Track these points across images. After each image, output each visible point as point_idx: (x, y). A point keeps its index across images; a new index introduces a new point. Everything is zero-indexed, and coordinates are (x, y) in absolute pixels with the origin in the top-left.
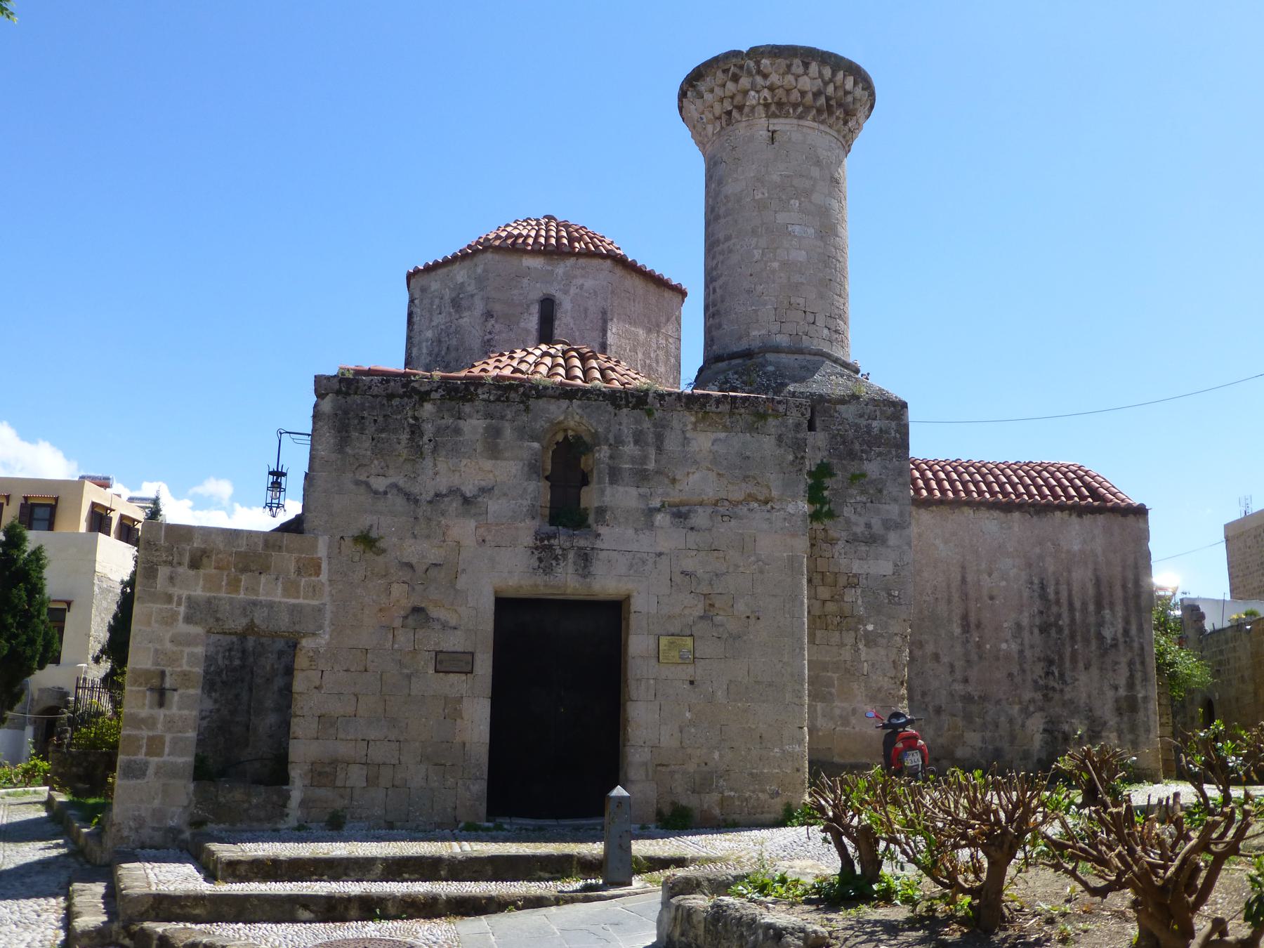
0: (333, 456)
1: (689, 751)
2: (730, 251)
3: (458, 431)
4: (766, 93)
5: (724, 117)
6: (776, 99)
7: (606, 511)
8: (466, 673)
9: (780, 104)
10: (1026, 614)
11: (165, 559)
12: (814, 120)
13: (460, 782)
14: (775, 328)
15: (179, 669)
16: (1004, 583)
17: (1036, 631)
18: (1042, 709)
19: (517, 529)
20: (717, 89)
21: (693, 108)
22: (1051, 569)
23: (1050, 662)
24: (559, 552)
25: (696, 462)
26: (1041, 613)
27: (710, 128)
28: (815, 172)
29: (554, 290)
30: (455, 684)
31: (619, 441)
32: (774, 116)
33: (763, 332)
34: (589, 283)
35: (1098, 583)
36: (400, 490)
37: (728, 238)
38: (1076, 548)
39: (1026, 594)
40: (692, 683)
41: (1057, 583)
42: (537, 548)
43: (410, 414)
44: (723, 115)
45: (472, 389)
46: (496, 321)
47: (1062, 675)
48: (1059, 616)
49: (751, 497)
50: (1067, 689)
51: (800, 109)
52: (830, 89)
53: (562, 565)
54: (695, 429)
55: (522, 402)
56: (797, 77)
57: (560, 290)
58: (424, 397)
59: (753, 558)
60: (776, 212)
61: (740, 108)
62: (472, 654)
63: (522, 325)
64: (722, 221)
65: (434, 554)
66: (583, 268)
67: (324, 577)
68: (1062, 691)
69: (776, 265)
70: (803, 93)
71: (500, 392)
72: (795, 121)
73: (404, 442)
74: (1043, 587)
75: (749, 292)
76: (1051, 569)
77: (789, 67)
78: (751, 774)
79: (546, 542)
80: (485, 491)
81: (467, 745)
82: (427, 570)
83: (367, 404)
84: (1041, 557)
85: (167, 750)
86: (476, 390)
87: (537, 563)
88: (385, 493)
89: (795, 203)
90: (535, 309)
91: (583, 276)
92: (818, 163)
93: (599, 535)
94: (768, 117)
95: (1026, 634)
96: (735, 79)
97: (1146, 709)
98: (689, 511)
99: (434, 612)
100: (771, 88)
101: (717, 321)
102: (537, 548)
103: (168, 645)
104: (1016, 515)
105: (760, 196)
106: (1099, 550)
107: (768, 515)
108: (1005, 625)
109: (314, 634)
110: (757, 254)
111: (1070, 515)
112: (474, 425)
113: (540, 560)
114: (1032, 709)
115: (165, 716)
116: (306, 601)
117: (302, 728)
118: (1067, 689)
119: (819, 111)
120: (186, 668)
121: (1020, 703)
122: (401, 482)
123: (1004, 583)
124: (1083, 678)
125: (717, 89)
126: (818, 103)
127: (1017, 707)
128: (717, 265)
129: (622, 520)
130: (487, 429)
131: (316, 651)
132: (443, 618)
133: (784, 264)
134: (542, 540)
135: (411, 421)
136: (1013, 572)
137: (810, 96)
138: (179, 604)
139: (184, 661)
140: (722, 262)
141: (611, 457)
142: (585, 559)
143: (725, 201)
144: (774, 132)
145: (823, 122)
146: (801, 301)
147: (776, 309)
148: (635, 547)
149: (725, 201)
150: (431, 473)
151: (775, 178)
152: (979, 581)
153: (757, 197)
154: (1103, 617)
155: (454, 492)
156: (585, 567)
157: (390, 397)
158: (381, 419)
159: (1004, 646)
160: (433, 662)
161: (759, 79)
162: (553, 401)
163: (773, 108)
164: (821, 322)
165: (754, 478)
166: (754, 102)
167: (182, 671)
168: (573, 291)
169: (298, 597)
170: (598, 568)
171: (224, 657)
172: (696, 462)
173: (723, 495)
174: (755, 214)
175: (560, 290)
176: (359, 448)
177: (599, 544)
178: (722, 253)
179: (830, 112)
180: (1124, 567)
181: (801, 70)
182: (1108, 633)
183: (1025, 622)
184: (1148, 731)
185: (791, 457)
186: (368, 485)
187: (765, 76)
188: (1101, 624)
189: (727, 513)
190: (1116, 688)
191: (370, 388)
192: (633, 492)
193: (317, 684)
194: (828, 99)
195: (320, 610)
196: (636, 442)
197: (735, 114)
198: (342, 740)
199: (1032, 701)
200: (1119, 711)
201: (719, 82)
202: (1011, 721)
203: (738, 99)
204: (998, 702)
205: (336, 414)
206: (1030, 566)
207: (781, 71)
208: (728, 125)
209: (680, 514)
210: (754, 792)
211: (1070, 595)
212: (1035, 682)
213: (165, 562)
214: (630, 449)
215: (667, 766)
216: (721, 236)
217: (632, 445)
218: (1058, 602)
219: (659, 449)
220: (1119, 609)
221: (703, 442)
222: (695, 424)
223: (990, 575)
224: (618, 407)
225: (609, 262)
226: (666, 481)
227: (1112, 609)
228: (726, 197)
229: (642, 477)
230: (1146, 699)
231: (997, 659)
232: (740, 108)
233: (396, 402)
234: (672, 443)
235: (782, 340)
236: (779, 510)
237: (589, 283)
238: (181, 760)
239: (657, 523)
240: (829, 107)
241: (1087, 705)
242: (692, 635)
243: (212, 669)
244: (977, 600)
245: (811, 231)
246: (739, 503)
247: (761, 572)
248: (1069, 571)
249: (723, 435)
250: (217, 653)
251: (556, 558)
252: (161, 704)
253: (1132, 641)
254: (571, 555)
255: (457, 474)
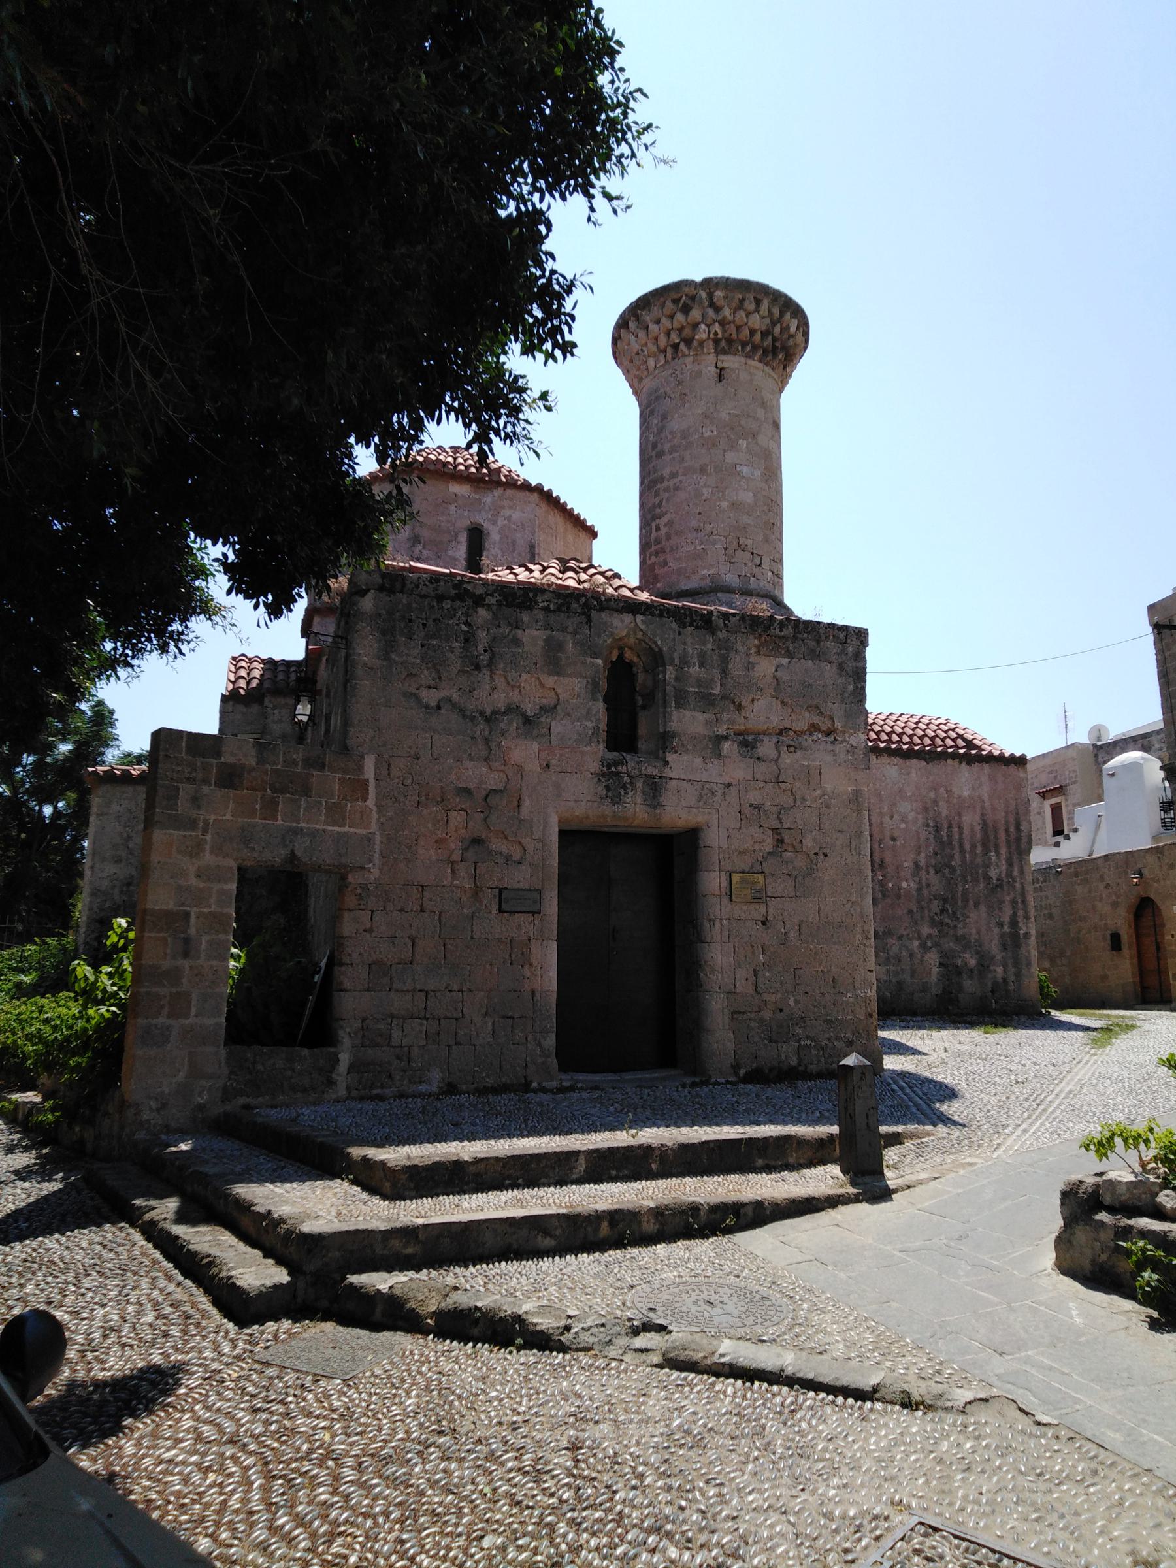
0: (378, 663)
1: (765, 996)
2: (677, 488)
3: (517, 642)
4: (717, 327)
5: (669, 350)
6: (726, 335)
7: (673, 737)
8: (533, 913)
9: (730, 341)
10: (923, 855)
11: (187, 775)
12: (760, 361)
13: (530, 1037)
14: (724, 568)
15: (206, 910)
16: (903, 826)
17: (932, 871)
18: (937, 945)
19: (583, 753)
20: (664, 320)
21: (632, 343)
22: (944, 813)
23: (945, 900)
24: (627, 780)
25: (760, 689)
26: (936, 854)
27: (651, 362)
28: (760, 413)
29: (481, 519)
30: (523, 925)
31: (685, 662)
32: (725, 353)
33: (712, 572)
34: (517, 515)
35: (984, 824)
36: (454, 705)
37: (674, 475)
38: (966, 793)
39: (923, 835)
40: (764, 923)
41: (950, 826)
42: (604, 775)
43: (463, 619)
44: (669, 349)
45: (531, 595)
46: (424, 548)
47: (954, 913)
48: (952, 857)
49: (814, 728)
50: (960, 925)
51: (748, 348)
52: (777, 330)
53: (631, 794)
54: (758, 653)
55: (584, 614)
56: (748, 314)
57: (489, 520)
58: (479, 601)
59: (818, 792)
60: (725, 451)
61: (688, 342)
62: (539, 891)
63: (450, 553)
64: (667, 458)
65: (494, 781)
66: (511, 500)
67: (371, 802)
68: (955, 927)
69: (725, 504)
70: (753, 332)
71: (560, 601)
72: (743, 360)
73: (458, 651)
74: (937, 830)
75: (697, 530)
76: (944, 813)
77: (742, 301)
78: (826, 1021)
79: (613, 769)
80: (548, 710)
81: (538, 995)
82: (487, 796)
83: (414, 605)
84: (936, 802)
85: (193, 1011)
86: (535, 596)
87: (605, 792)
88: (439, 707)
89: (743, 443)
90: (463, 538)
91: (510, 508)
92: (763, 405)
93: (667, 763)
94: (717, 353)
95: (923, 874)
96: (686, 310)
97: (1027, 945)
98: (755, 740)
99: (496, 845)
100: (723, 323)
101: (662, 559)
102: (604, 775)
103: (193, 881)
104: (914, 762)
105: (709, 433)
106: (986, 797)
107: (831, 748)
108: (905, 865)
109: (362, 868)
110: (706, 493)
111: (960, 763)
112: (532, 636)
113: (607, 788)
114: (929, 944)
115: (191, 967)
116: (352, 830)
117: (352, 978)
118: (960, 925)
119: (765, 352)
120: (213, 908)
121: (919, 938)
122: (455, 696)
123: (903, 826)
124: (973, 916)
125: (664, 320)
126: (765, 344)
127: (916, 943)
128: (661, 501)
129: (690, 747)
130: (548, 641)
131: (365, 888)
132: (505, 851)
133: (734, 505)
134: (609, 766)
135: (465, 628)
136: (911, 816)
137: (758, 337)
138: (205, 831)
139: (212, 901)
140: (668, 500)
141: (677, 679)
142: (655, 789)
143: (670, 437)
144: (722, 369)
145: (766, 364)
146: (749, 542)
147: (725, 549)
148: (704, 776)
149: (670, 437)
150: (487, 687)
151: (724, 416)
152: (882, 823)
153: (706, 435)
154: (990, 859)
155: (512, 710)
156: (654, 797)
157: (441, 598)
158: (430, 623)
159: (904, 885)
160: (497, 900)
161: (711, 312)
162: (616, 615)
163: (723, 343)
164: (765, 566)
165: (817, 707)
166: (704, 336)
167: (210, 913)
168: (501, 522)
169: (344, 825)
170: (668, 799)
171: (121, 892)
172: (760, 689)
173: (787, 724)
174: (703, 451)
175: (489, 520)
176: (407, 655)
177: (668, 773)
178: (667, 490)
179: (775, 354)
180: (1006, 813)
181: (752, 307)
182: (993, 873)
183: (922, 862)
184: (1029, 965)
185: (851, 687)
186: (418, 699)
187: (717, 310)
188: (987, 866)
189: (792, 743)
190: (1001, 925)
191: (417, 586)
192: (701, 717)
193: (368, 926)
194: (774, 340)
195: (369, 839)
196: (702, 665)
197: (682, 347)
198: (397, 991)
199: (929, 936)
200: (1004, 947)
201: (667, 311)
202: (912, 955)
203: (687, 332)
204: (900, 937)
205: (380, 615)
206: (926, 809)
207: (734, 305)
208: (673, 359)
209: (747, 742)
210: (829, 1040)
211: (961, 838)
212: (932, 919)
213: (188, 779)
214: (695, 670)
215: (744, 1013)
216: (666, 472)
217: (697, 666)
218: (950, 842)
219: (724, 673)
220: (1003, 850)
221: (765, 667)
222: (758, 647)
223: (892, 817)
224: (683, 625)
225: (536, 495)
226: (732, 707)
227: (997, 852)
228: (671, 433)
229: (707, 701)
230: (1027, 935)
231: (898, 897)
232: (688, 342)
233: (447, 605)
234: (736, 669)
235: (731, 579)
236: (841, 743)
237: (517, 515)
238: (209, 1022)
239: (724, 753)
240: (774, 348)
241: (977, 940)
242: (762, 872)
243: (107, 905)
244: (881, 841)
245: (757, 473)
246: (802, 733)
247: (828, 807)
248: (960, 815)
249: (785, 661)
250: (113, 887)
251: (624, 787)
252: (186, 955)
253: (1014, 881)
254: (639, 785)
255: (517, 691)
